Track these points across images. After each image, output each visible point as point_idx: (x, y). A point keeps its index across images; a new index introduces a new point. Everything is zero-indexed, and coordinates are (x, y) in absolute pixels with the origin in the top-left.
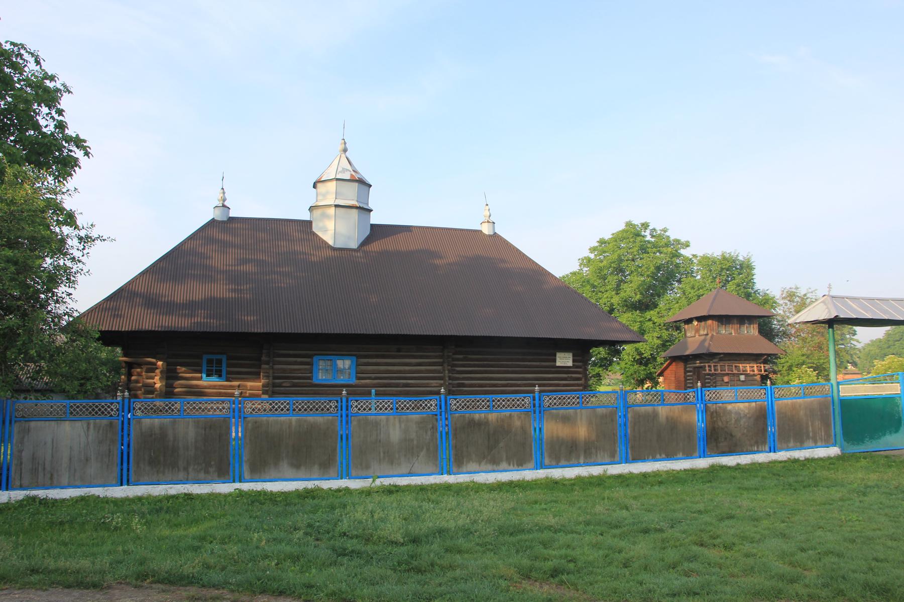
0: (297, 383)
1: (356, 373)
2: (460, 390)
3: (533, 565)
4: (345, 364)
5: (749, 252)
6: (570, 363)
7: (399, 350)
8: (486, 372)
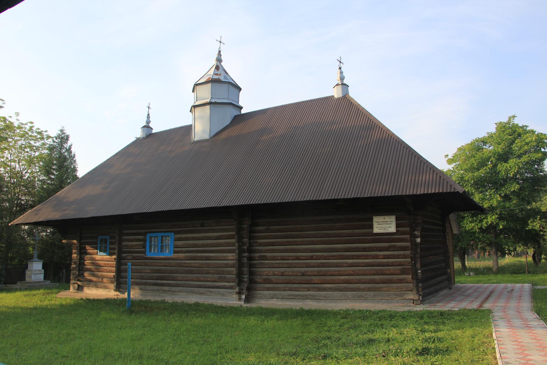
0: (136, 256)
1: (174, 248)
2: (262, 263)
3: (506, 286)
4: (170, 240)
5: (514, 117)
6: (392, 229)
7: (202, 225)
8: (289, 244)
